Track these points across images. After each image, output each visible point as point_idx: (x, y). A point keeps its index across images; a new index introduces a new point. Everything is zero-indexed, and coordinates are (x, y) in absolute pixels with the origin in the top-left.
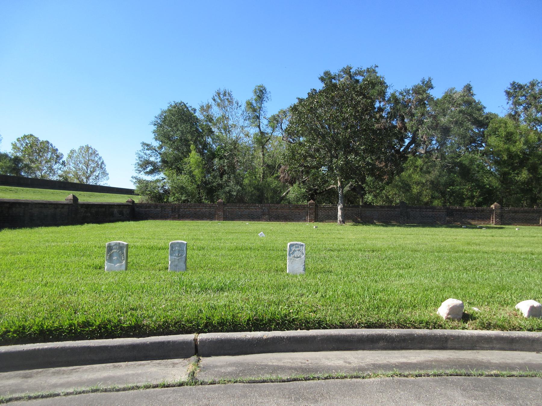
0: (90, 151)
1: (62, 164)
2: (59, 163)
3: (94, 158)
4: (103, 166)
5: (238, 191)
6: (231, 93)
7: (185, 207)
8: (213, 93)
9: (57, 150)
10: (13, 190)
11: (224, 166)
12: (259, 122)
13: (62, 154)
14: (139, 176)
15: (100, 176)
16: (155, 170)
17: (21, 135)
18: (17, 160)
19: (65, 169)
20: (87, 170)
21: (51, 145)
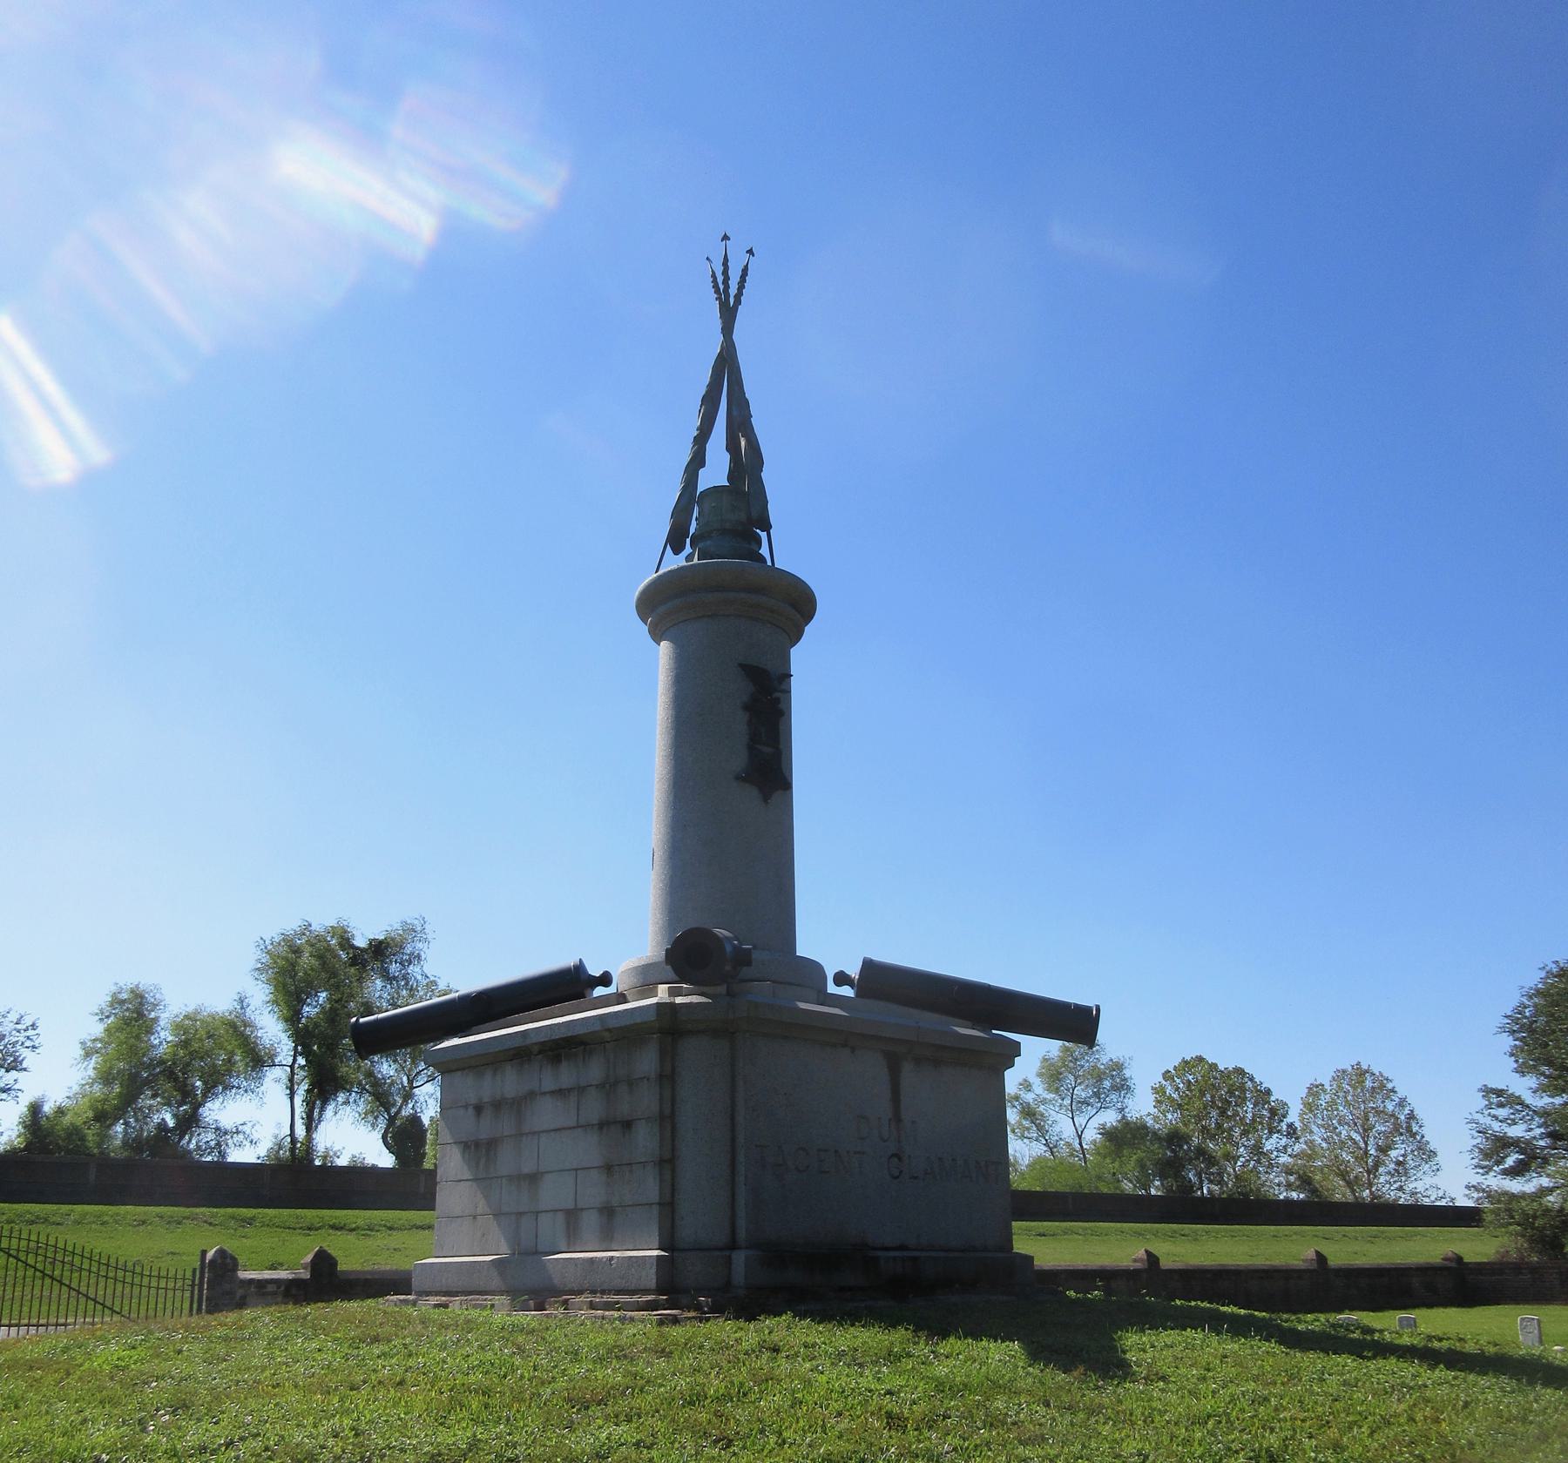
0: (1368, 1084)
1: (1289, 1135)
4: (1415, 1128)
9: (1268, 1092)
10: (1187, 1233)
16: (1530, 1161)
17: (1171, 1064)
18: (1175, 1138)
19: (1298, 1147)
21: (1252, 1079)
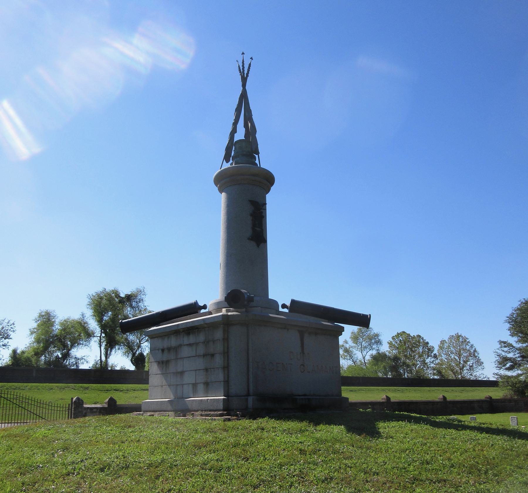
0: (461, 340)
2: (431, 356)
3: (466, 346)
4: (476, 355)
9: (428, 343)
13: (433, 347)
14: (500, 372)
15: (475, 366)
18: (396, 359)
20: (460, 360)
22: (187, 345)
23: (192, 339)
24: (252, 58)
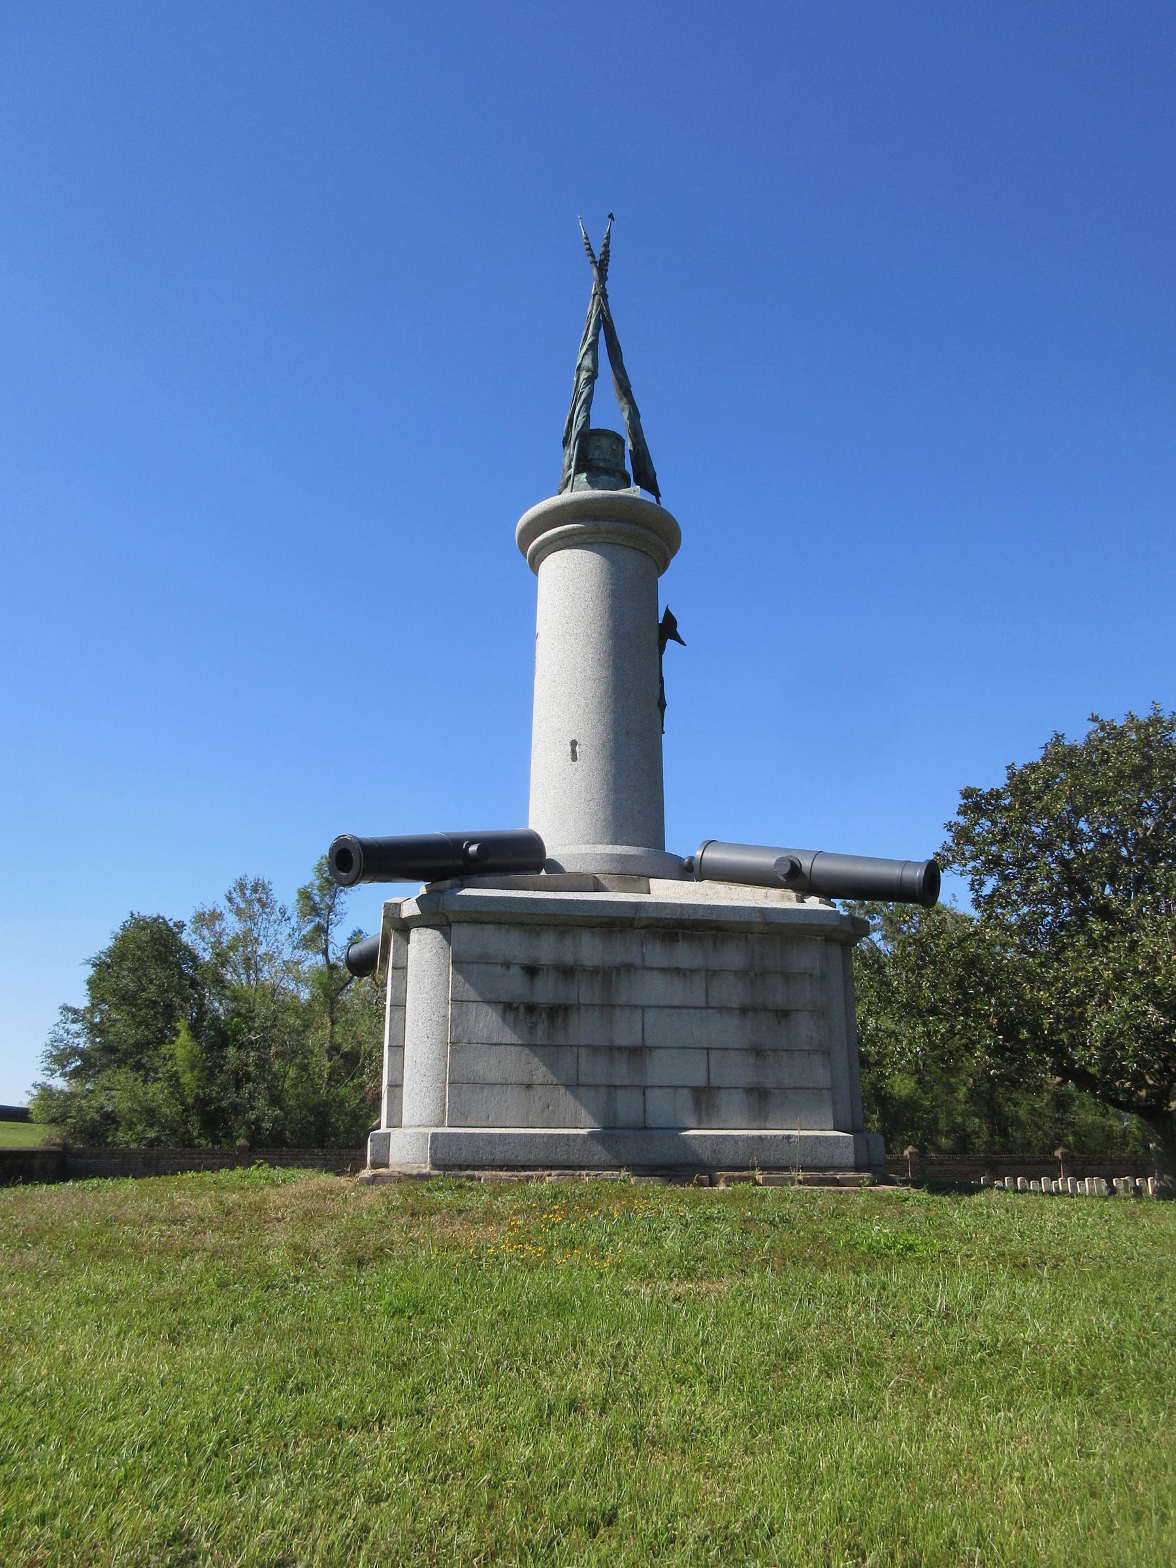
5: (276, 1120)
6: (271, 887)
7: (172, 1156)
8: (229, 884)
11: (247, 1065)
12: (326, 941)
14: (49, 1083)
22: (664, 969)
23: (685, 955)
24: (611, 216)
